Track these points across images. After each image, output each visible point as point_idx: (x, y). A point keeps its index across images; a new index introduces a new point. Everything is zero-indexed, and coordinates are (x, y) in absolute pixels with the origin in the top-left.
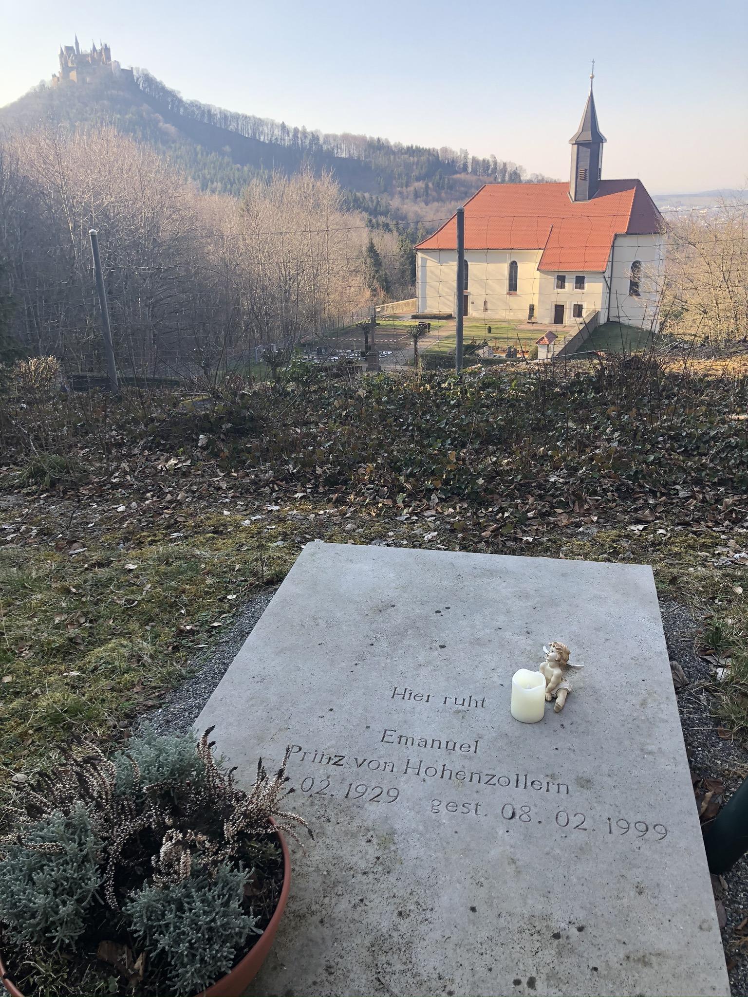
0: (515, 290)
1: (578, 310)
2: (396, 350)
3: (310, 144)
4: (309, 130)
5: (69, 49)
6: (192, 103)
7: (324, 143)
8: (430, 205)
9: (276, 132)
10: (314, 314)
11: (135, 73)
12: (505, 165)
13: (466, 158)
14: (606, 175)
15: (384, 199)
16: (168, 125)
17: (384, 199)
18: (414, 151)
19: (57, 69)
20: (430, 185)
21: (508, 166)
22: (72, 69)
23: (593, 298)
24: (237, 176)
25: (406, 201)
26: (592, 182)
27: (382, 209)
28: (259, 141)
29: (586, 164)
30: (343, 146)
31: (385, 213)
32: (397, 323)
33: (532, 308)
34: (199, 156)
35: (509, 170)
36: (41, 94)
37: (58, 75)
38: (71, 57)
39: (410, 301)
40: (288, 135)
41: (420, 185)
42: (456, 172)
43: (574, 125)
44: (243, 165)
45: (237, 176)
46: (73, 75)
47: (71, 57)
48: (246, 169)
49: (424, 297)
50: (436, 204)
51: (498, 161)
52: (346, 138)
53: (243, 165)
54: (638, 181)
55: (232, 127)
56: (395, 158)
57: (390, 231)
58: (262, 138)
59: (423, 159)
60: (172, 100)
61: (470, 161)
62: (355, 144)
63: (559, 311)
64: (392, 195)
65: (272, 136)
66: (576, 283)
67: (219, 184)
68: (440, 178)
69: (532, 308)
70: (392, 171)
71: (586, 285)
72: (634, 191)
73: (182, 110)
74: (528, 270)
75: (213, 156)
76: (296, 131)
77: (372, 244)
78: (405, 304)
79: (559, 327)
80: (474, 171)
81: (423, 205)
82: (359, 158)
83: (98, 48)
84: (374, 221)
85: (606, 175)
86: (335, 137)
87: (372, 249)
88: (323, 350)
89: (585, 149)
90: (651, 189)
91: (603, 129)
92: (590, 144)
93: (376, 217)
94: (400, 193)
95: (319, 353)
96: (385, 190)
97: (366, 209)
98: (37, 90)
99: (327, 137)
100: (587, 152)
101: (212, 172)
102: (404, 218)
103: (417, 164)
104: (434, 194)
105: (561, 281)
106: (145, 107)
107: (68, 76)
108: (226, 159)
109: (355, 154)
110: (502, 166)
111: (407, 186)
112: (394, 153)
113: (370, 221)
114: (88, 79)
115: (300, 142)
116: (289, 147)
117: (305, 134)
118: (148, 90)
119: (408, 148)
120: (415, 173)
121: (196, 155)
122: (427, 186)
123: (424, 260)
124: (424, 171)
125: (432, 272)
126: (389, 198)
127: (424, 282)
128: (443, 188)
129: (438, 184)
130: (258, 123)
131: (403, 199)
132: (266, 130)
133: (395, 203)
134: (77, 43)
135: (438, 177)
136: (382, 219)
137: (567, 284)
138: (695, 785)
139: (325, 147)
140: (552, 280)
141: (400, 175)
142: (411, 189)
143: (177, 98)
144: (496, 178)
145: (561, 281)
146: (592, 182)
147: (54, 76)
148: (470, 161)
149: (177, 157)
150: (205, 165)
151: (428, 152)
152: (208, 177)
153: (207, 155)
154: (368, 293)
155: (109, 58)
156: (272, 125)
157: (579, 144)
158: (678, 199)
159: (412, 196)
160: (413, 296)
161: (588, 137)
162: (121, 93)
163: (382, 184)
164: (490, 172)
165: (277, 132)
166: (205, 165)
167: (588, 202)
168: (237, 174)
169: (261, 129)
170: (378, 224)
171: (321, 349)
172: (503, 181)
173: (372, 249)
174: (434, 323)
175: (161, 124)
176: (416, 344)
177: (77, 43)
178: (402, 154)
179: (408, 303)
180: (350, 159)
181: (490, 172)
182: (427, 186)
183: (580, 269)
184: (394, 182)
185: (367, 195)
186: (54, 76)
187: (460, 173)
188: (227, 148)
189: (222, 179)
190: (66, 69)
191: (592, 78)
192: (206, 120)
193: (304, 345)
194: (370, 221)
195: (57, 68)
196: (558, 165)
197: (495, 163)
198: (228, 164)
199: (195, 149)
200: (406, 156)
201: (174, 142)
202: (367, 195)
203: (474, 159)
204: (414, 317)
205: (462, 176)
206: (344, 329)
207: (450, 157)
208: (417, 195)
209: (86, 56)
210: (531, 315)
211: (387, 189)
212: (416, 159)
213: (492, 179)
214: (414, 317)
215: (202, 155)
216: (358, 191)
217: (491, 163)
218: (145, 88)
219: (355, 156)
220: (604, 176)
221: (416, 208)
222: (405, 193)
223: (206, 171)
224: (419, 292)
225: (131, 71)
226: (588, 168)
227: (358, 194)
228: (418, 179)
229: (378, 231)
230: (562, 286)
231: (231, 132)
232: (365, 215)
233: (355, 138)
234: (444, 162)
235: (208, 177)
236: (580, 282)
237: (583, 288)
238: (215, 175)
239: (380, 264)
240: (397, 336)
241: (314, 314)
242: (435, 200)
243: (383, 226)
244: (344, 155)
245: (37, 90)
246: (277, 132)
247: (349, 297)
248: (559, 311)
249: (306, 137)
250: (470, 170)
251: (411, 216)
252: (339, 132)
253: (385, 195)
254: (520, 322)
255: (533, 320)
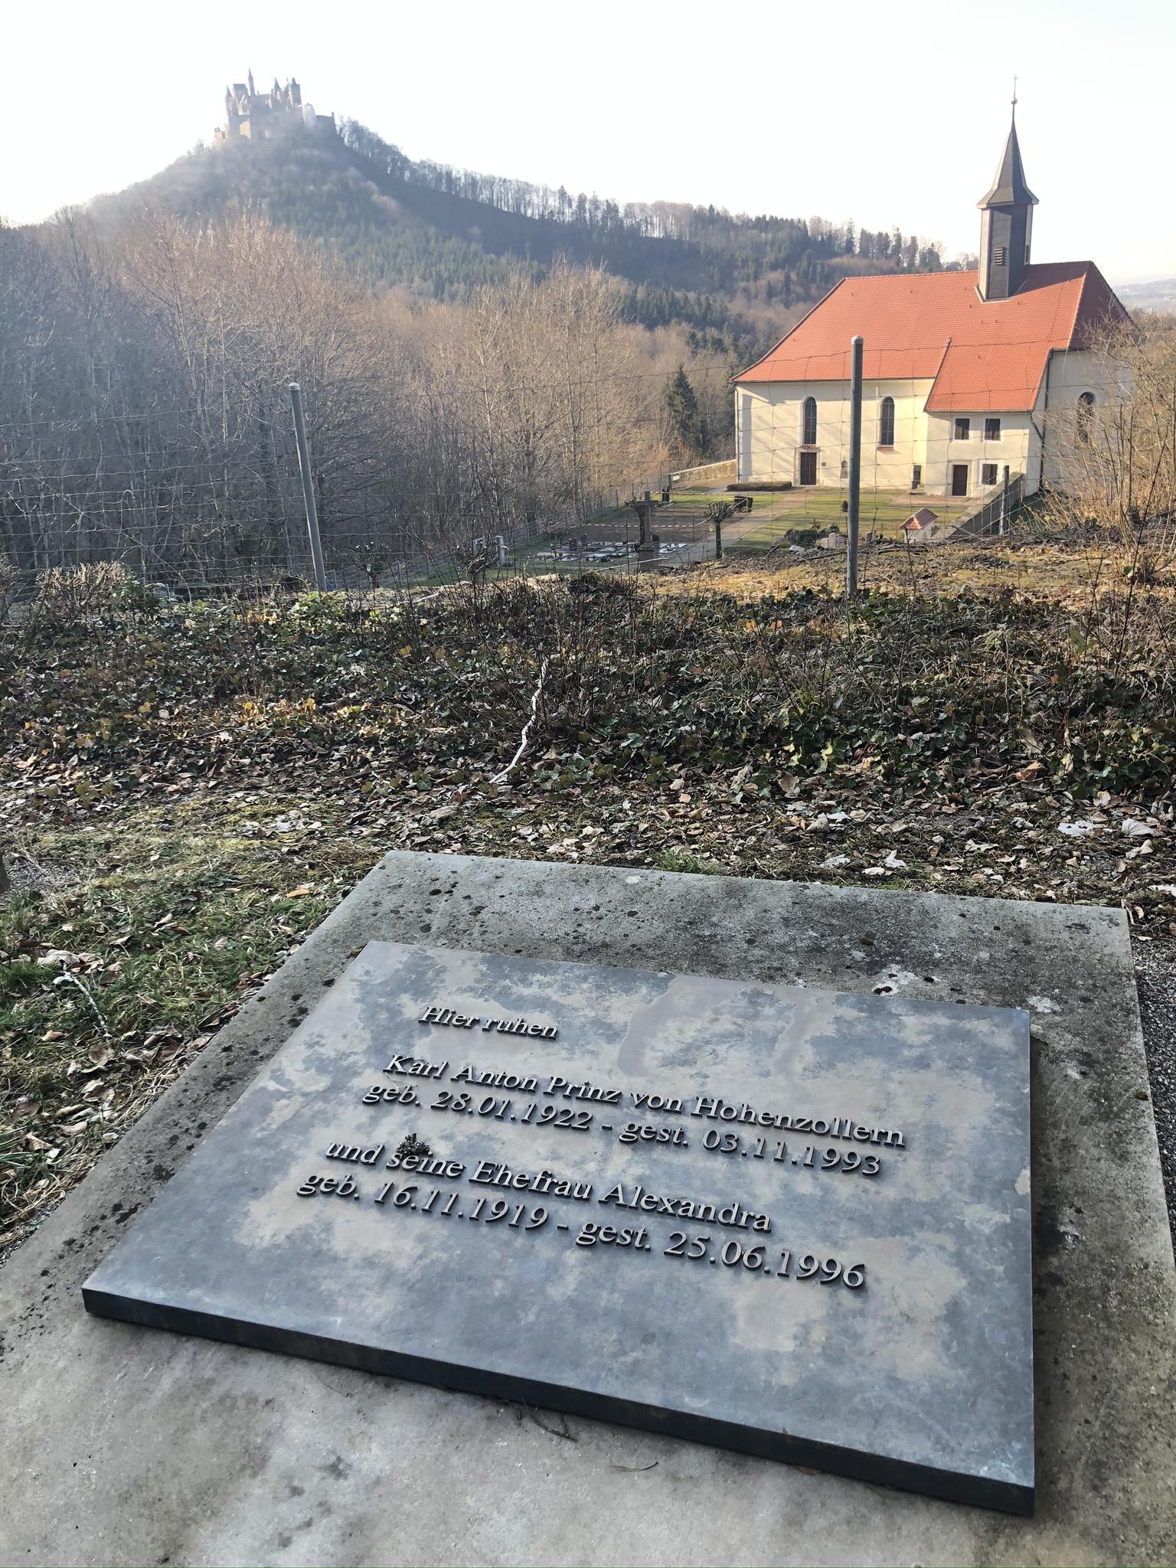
0: (892, 443)
1: (990, 473)
2: (694, 540)
3: (604, 218)
4: (602, 198)
5: (239, 87)
6: (422, 162)
7: (626, 215)
8: (792, 308)
9: (551, 202)
10: (569, 493)
11: (338, 122)
12: (914, 239)
13: (850, 230)
14: (1040, 254)
15: (719, 300)
16: (385, 199)
17: (719, 300)
18: (767, 224)
19: (223, 121)
20: (793, 276)
21: (919, 242)
22: (243, 119)
23: (1013, 451)
24: (489, 272)
25: (754, 302)
26: (1014, 269)
27: (715, 316)
28: (524, 217)
29: (1005, 239)
30: (656, 220)
31: (719, 325)
32: (701, 497)
33: (917, 472)
34: (433, 243)
35: (920, 247)
36: (204, 159)
37: (223, 129)
38: (247, 103)
39: (729, 462)
40: (570, 206)
41: (776, 276)
42: (835, 255)
43: (987, 178)
44: (498, 255)
45: (489, 272)
46: (245, 128)
47: (247, 103)
48: (503, 260)
49: (748, 453)
50: (801, 306)
51: (903, 235)
52: (661, 208)
53: (498, 255)
54: (1091, 264)
55: (484, 196)
56: (736, 236)
57: (724, 351)
58: (529, 213)
59: (782, 235)
60: (393, 160)
61: (857, 235)
62: (674, 215)
63: (960, 473)
64: (732, 293)
65: (545, 207)
66: (987, 430)
67: (462, 285)
68: (809, 265)
69: (917, 472)
70: (733, 256)
71: (1002, 433)
72: (1083, 280)
73: (407, 174)
74: (910, 411)
75: (453, 243)
76: (582, 200)
77: (681, 373)
78: (719, 468)
79: (958, 500)
80: (864, 252)
81: (781, 307)
82: (680, 237)
83: (283, 85)
84: (699, 335)
85: (1040, 254)
86: (643, 207)
87: (681, 382)
88: (580, 543)
89: (1002, 215)
90: (1114, 276)
91: (1032, 183)
92: (1012, 207)
93: (703, 330)
94: (745, 290)
95: (573, 547)
96: (722, 287)
97: (689, 318)
98: (193, 152)
99: (630, 207)
100: (1006, 219)
101: (452, 266)
102: (750, 329)
103: (772, 243)
104: (799, 290)
105: (962, 427)
106: (352, 172)
107: (238, 129)
108: (473, 247)
109: (674, 230)
110: (909, 243)
111: (756, 279)
112: (735, 227)
113: (693, 336)
114: (267, 134)
115: (587, 215)
116: (571, 225)
117: (595, 204)
118: (356, 145)
119: (758, 219)
120: (770, 257)
121: (428, 241)
122: (788, 278)
123: (748, 400)
124: (783, 254)
125: (760, 418)
126: (727, 298)
127: (748, 431)
128: (814, 280)
129: (806, 274)
130: (523, 191)
131: (749, 299)
132: (536, 200)
133: (736, 306)
134: (251, 78)
135: (805, 264)
136: (712, 332)
137: (971, 433)
138: (1035, 1291)
139: (627, 222)
140: (947, 425)
141: (745, 262)
142: (762, 283)
143: (400, 155)
144: (899, 262)
145: (962, 427)
146: (1014, 269)
147: (217, 130)
148: (857, 235)
149: (399, 246)
150: (441, 256)
151: (790, 224)
152: (445, 275)
153: (444, 241)
154: (663, 452)
155: (298, 100)
156: (545, 190)
157: (995, 208)
158: (1152, 290)
159: (763, 295)
160: (731, 455)
161: (1009, 196)
162: (316, 152)
163: (717, 276)
164: (889, 252)
165: (553, 202)
166: (441, 256)
167: (1008, 300)
168: (490, 269)
169: (528, 198)
170: (705, 341)
171: (575, 541)
172: (911, 264)
173: (681, 382)
174: (757, 497)
175: (375, 197)
176: (718, 530)
177: (251, 78)
178: (749, 228)
179: (725, 467)
180: (666, 240)
181: (889, 252)
182: (788, 278)
183: (999, 404)
184: (736, 274)
185: (692, 295)
186: (217, 130)
187: (841, 255)
188: (476, 230)
189: (467, 277)
190: (235, 119)
191: (1014, 103)
192: (443, 188)
193: (552, 536)
194: (693, 336)
195: (222, 119)
196: (963, 238)
197: (899, 238)
198: (476, 254)
199: (426, 233)
200: (755, 232)
201: (394, 223)
202: (692, 295)
203: (863, 233)
204: (732, 488)
205: (844, 261)
206: (617, 509)
207: (825, 229)
208: (771, 293)
209: (266, 96)
210: (916, 482)
211: (725, 285)
212: (770, 236)
213: (893, 263)
214: (732, 488)
215: (437, 240)
216: (678, 289)
217: (892, 238)
218: (352, 143)
219: (675, 236)
220: (1035, 260)
221: (769, 314)
222: (753, 291)
223: (442, 267)
224: (740, 448)
225: (332, 119)
226: (1007, 246)
227: (678, 295)
228: (774, 267)
229: (704, 352)
230: (964, 435)
231: (481, 205)
232: (686, 327)
233: (673, 206)
234: (815, 240)
235: (445, 275)
236: (993, 428)
237: (998, 438)
238: (456, 271)
239: (695, 406)
240: (694, 519)
241: (569, 493)
242: (800, 299)
243: (713, 344)
244: (656, 234)
245: (193, 152)
246: (553, 202)
247: (630, 459)
248: (960, 473)
249: (597, 208)
250: (857, 250)
251: (761, 326)
252: (650, 201)
253: (722, 293)
254: (899, 492)
255: (919, 489)
